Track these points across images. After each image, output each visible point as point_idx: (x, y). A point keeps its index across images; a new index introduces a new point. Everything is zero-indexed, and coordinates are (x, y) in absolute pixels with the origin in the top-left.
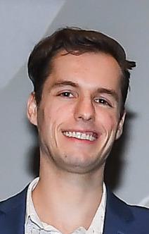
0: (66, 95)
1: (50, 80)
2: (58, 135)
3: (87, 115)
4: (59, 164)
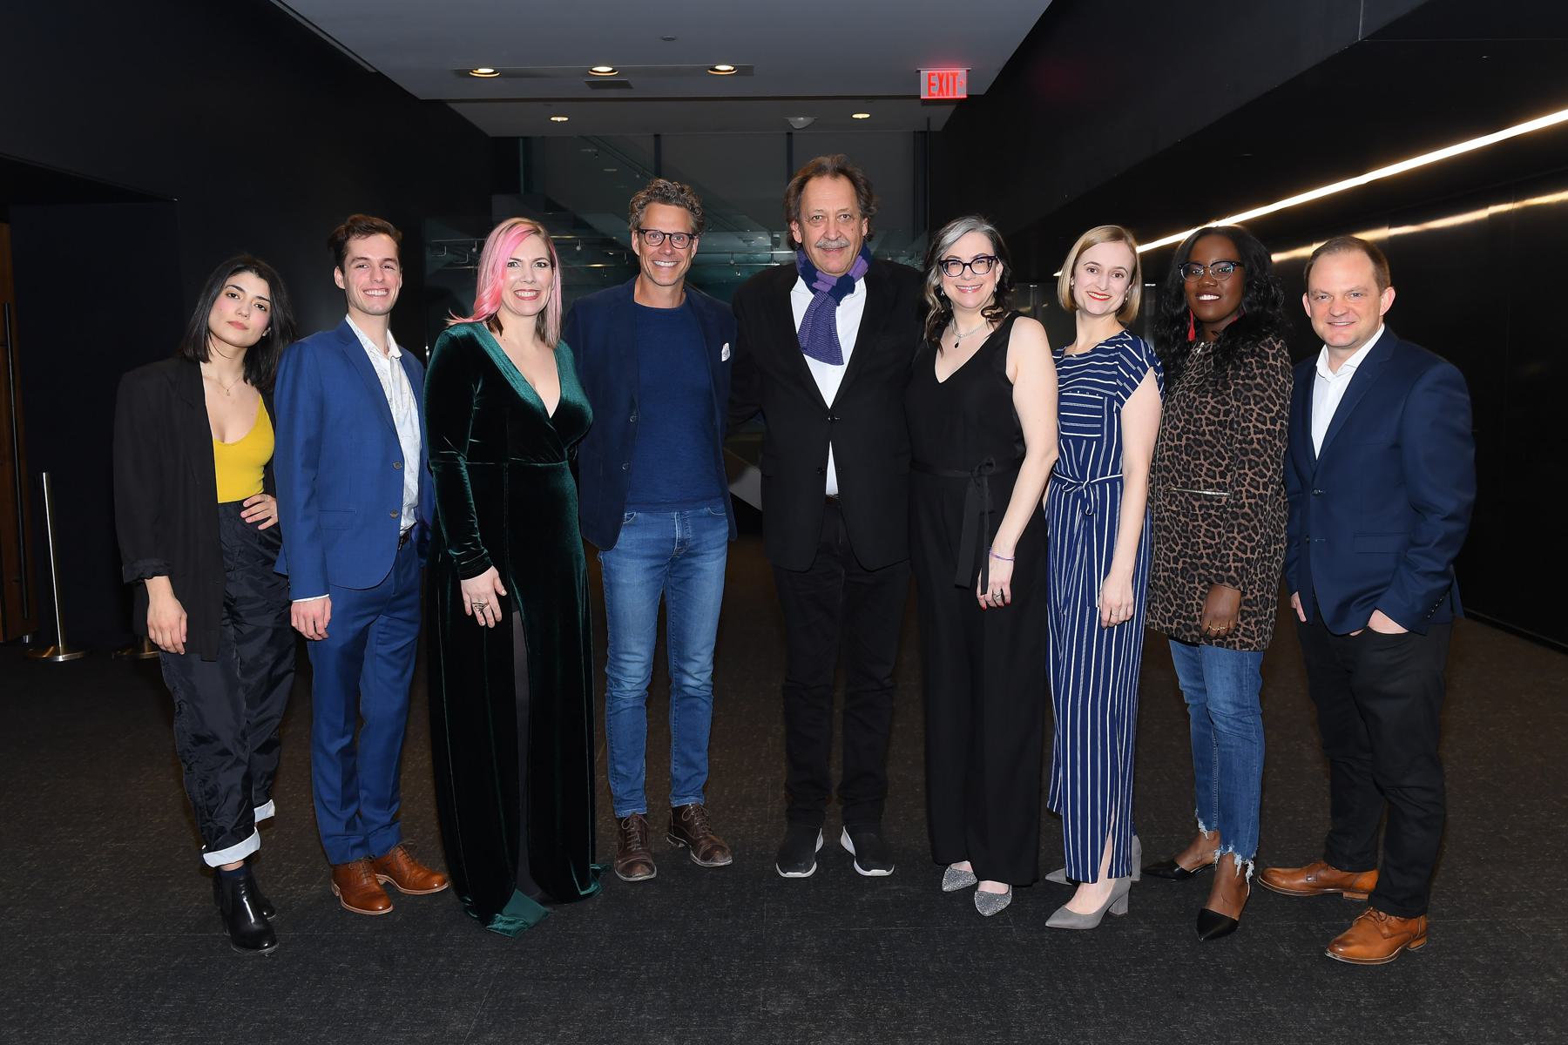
1: (349, 258)
2: (361, 294)
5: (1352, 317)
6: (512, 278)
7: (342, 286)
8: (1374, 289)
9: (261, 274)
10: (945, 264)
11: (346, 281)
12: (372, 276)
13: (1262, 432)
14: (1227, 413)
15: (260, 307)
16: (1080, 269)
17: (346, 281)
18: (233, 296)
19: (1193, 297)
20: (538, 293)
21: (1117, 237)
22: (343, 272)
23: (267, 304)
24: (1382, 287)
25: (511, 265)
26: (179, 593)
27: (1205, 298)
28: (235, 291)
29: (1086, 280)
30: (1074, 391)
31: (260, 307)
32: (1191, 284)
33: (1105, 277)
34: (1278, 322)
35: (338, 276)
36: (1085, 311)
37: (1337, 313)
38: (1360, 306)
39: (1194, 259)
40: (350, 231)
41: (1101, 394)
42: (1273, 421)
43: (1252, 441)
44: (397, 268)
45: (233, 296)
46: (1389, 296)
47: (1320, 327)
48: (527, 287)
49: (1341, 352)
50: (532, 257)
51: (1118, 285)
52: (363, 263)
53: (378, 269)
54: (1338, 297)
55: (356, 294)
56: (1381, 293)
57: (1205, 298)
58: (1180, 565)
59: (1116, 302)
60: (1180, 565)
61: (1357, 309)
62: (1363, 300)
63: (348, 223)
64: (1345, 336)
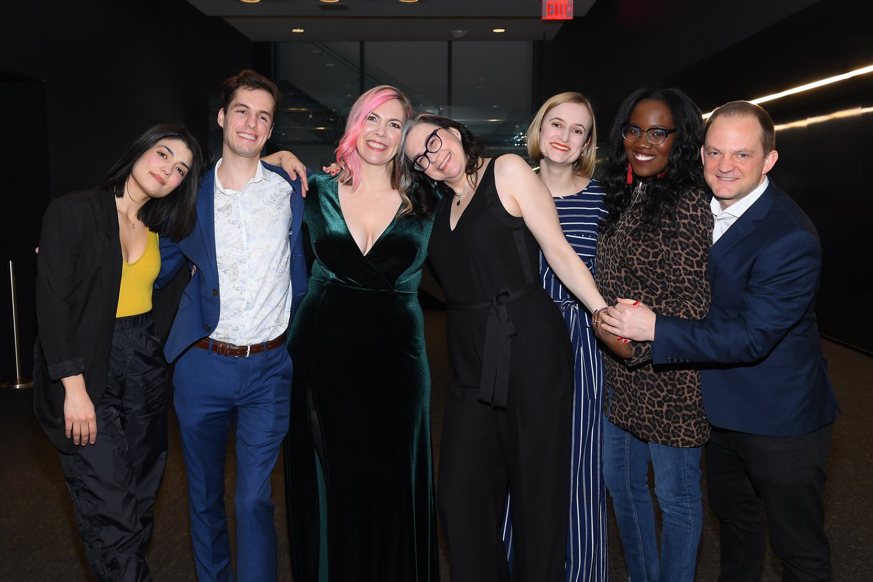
0: (243, 112)
1: (233, 102)
2: (235, 134)
3: (252, 125)
4: (234, 151)
5: (737, 174)
6: (369, 129)
7: (221, 124)
8: (760, 152)
9: (190, 146)
10: (667, 132)
11: (226, 121)
12: (247, 122)
13: (690, 273)
14: (655, 255)
15: (180, 170)
16: (547, 125)
17: (226, 121)
18: (162, 155)
19: (630, 153)
20: (386, 147)
21: (578, 100)
22: (225, 113)
23: (185, 170)
24: (766, 151)
25: (372, 119)
26: (91, 390)
27: (641, 158)
28: (165, 151)
29: (551, 132)
30: (579, 234)
31: (180, 170)
32: (629, 140)
33: (567, 131)
34: (686, 175)
35: (221, 115)
36: (550, 162)
37: (725, 170)
38: (745, 165)
39: (633, 121)
40: (240, 83)
41: (593, 236)
42: (699, 264)
43: (683, 281)
44: (269, 120)
45: (162, 155)
46: (772, 159)
47: (710, 178)
48: (378, 139)
49: (726, 202)
50: (389, 117)
51: (577, 140)
52: (244, 110)
53: (253, 117)
54: (727, 156)
55: (231, 135)
56: (766, 155)
57: (641, 158)
58: (665, 408)
59: (574, 155)
60: (665, 408)
61: (742, 167)
62: (749, 161)
63: (241, 74)
64: (729, 190)
